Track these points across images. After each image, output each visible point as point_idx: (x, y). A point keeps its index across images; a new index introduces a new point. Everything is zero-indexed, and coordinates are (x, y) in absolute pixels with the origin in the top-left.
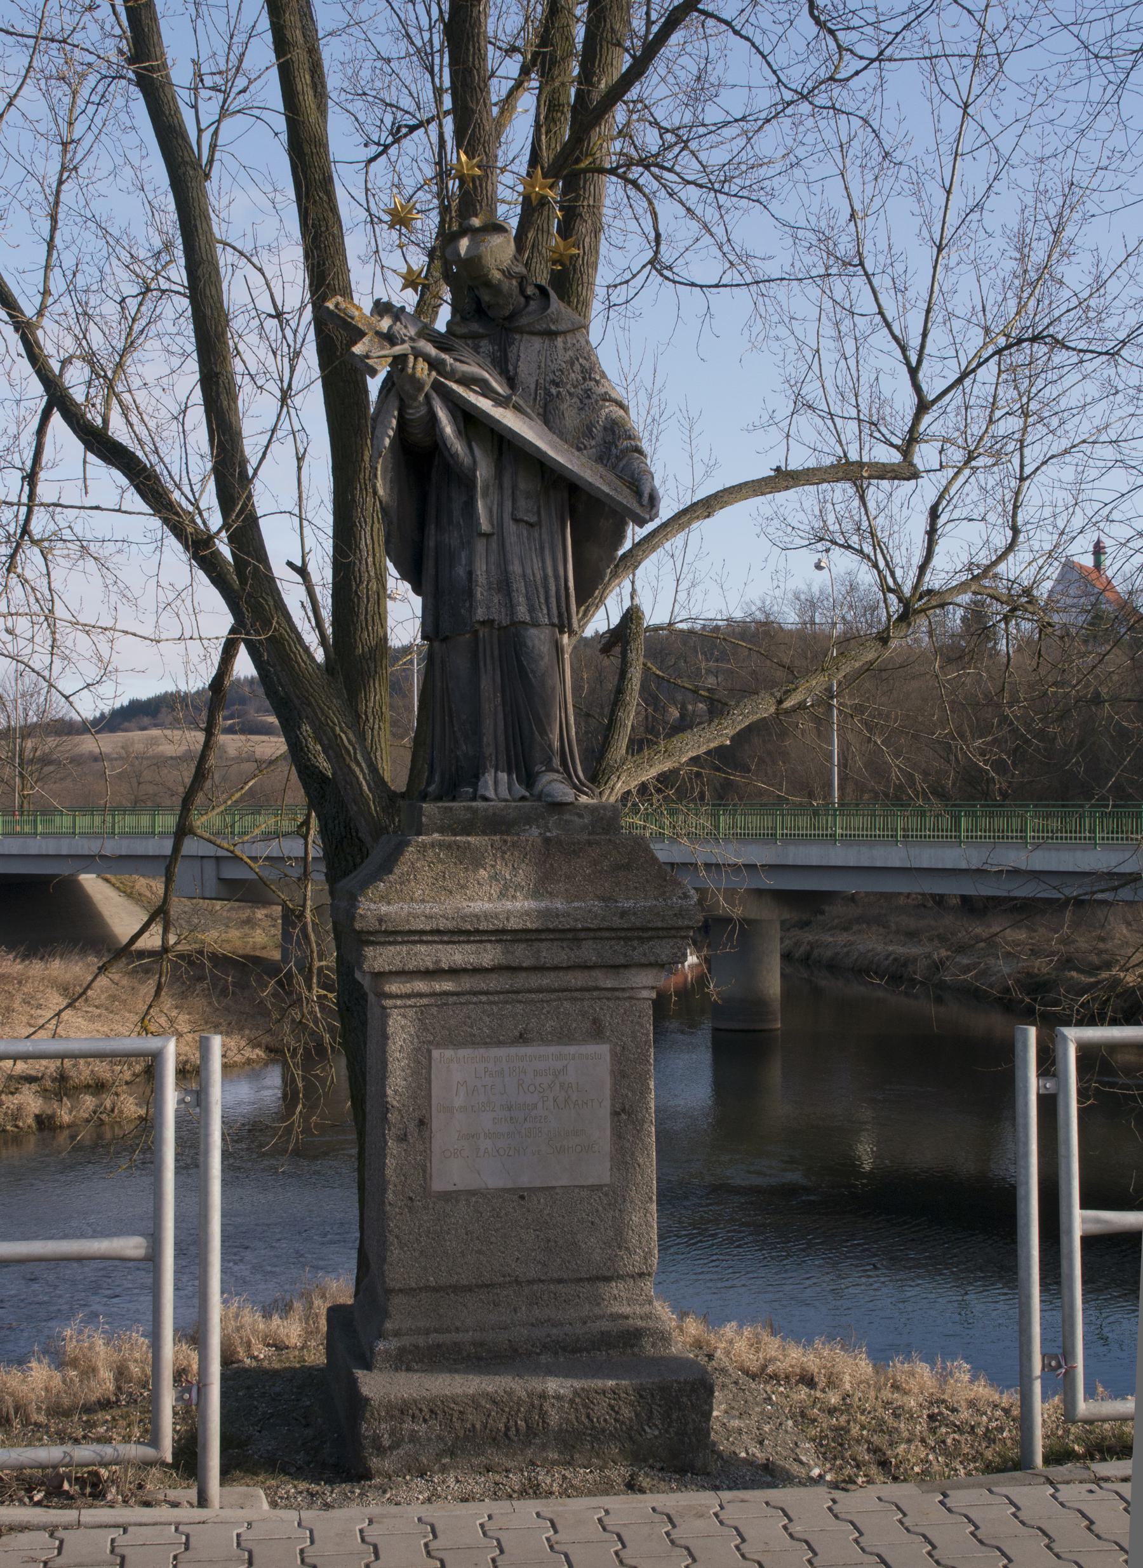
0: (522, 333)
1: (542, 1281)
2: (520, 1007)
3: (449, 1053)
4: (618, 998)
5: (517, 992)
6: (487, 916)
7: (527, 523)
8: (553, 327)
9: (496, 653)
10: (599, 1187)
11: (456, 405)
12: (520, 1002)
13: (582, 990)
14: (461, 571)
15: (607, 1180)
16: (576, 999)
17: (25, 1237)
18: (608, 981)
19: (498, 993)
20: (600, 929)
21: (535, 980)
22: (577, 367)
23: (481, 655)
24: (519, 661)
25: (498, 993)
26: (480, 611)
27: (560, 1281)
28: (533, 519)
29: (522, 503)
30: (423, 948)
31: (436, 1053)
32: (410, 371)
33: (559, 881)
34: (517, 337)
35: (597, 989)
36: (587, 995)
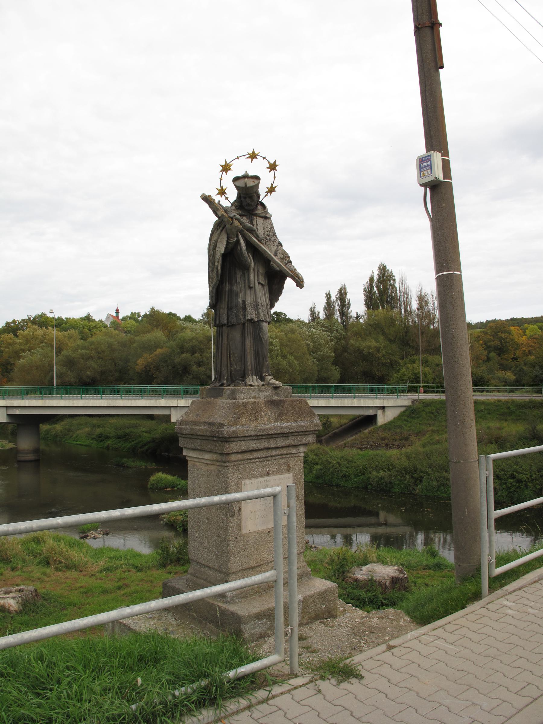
2: (267, 462)
16: (283, 458)
17: (58, 621)
18: (293, 451)
29: (260, 277)
30: (243, 443)
31: (243, 482)
32: (428, 190)
33: (283, 416)
34: (255, 217)
35: (291, 454)
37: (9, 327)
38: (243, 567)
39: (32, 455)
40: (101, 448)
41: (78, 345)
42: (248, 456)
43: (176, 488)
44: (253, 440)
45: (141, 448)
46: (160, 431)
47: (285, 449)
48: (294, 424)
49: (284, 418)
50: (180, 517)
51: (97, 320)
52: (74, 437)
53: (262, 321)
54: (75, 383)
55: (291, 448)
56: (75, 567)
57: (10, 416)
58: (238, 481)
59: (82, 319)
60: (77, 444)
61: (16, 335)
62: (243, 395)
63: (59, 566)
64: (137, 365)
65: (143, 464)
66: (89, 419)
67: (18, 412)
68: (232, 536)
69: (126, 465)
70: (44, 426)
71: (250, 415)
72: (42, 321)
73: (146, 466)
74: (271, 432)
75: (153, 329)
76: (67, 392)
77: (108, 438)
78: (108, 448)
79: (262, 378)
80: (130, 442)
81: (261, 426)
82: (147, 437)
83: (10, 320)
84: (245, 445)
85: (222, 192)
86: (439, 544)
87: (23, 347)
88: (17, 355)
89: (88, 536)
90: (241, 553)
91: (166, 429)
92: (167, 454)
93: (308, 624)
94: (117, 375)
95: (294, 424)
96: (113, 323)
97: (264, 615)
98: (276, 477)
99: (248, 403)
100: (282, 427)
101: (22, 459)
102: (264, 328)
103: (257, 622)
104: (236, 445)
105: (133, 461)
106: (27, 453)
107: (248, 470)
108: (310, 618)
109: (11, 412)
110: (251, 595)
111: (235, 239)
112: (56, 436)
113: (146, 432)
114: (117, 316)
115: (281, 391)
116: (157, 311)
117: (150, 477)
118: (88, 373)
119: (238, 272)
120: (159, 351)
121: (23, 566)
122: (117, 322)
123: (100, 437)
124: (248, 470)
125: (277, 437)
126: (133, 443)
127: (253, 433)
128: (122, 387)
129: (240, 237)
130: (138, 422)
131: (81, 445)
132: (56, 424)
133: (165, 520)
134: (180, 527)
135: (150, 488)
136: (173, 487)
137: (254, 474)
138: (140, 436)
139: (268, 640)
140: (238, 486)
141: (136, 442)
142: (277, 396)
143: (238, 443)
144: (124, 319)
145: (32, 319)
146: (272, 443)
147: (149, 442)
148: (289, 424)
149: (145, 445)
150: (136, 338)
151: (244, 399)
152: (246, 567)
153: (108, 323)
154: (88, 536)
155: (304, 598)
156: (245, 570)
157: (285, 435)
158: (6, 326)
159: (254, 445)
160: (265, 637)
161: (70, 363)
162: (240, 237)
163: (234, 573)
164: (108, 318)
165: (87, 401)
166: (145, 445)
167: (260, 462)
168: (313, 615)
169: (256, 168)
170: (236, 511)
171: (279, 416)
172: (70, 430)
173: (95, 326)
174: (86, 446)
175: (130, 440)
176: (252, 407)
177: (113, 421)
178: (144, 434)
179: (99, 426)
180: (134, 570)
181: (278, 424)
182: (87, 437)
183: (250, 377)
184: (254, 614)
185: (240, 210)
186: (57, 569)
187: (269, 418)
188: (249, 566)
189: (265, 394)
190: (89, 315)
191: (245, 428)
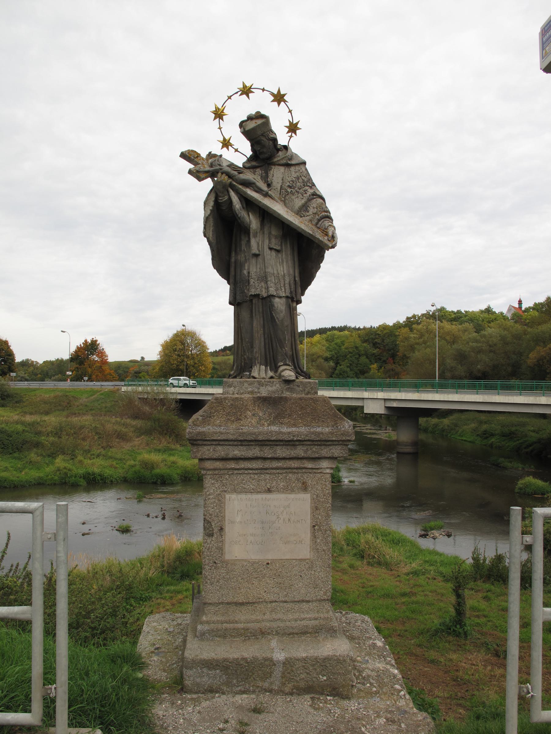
0: (275, 165)
1: (277, 602)
3: (234, 496)
4: (315, 473)
5: (266, 469)
6: (251, 434)
7: (276, 250)
8: (289, 162)
9: (261, 310)
10: (305, 560)
11: (241, 195)
12: (268, 474)
13: (297, 468)
14: (245, 272)
15: (308, 557)
16: (295, 473)
19: (257, 469)
20: (305, 441)
21: (275, 464)
22: (300, 180)
23: (254, 311)
24: (271, 314)
25: (257, 469)
26: (253, 290)
27: (285, 602)
28: (278, 248)
29: (273, 240)
30: (220, 448)
31: (227, 496)
33: (284, 418)
36: (300, 471)
37: (409, 321)
38: (225, 599)
39: (410, 447)
40: (485, 445)
41: (469, 338)
42: (233, 465)
44: (236, 445)
45: (525, 448)
47: (295, 461)
48: (303, 430)
49: (286, 420)
51: (497, 312)
52: (459, 432)
53: (273, 296)
54: (466, 377)
55: (305, 461)
56: (387, 565)
57: (388, 408)
58: (219, 495)
59: (482, 312)
60: (462, 440)
61: (411, 330)
62: (232, 388)
63: (371, 560)
65: (521, 466)
66: (477, 415)
67: (395, 405)
68: (209, 560)
69: (502, 465)
70: (433, 420)
71: (228, 414)
72: (441, 315)
74: (260, 438)
76: (390, 385)
77: (492, 435)
78: (491, 445)
79: (275, 368)
80: (515, 441)
81: (245, 429)
82: (534, 437)
83: (410, 316)
84: (221, 451)
85: (226, 144)
87: (417, 341)
88: (412, 348)
89: (427, 535)
93: (292, 694)
94: (510, 369)
95: (303, 430)
96: (514, 315)
97: (217, 665)
98: (282, 496)
99: (225, 398)
100: (281, 433)
101: (401, 451)
102: (276, 305)
103: (205, 670)
104: (209, 450)
105: (511, 462)
106: (406, 446)
107: (236, 482)
108: (295, 687)
109: (389, 404)
110: (231, 636)
111: (226, 198)
112: (443, 430)
113: (534, 431)
114: (520, 308)
115: (298, 386)
118: (479, 367)
119: (243, 237)
121: (340, 555)
122: (519, 315)
123: (485, 434)
124: (236, 482)
125: (277, 445)
126: (518, 442)
127: (231, 437)
128: (513, 382)
129: (232, 194)
130: (528, 420)
131: (465, 441)
132: (445, 418)
135: (518, 493)
137: (245, 488)
138: (526, 436)
139: (219, 697)
140: (219, 500)
141: (520, 441)
142: (291, 392)
143: (212, 448)
144: (527, 310)
145: (431, 313)
146: (267, 452)
147: (535, 443)
148: (294, 429)
149: (530, 446)
151: (233, 394)
152: (229, 600)
153: (509, 316)
154: (427, 535)
155: (286, 659)
156: (228, 603)
157: (291, 443)
158: (407, 321)
159: (237, 452)
160: (217, 692)
161: (461, 357)
162: (232, 194)
163: (210, 604)
164: (509, 310)
165: (462, 396)
167: (256, 474)
168: (302, 684)
169: (261, 103)
171: (278, 418)
172: (456, 425)
173: (495, 319)
174: (470, 442)
175: (515, 439)
176: (232, 405)
177: (501, 418)
179: (486, 423)
180: (441, 579)
181: (274, 428)
182: (472, 432)
183: (258, 366)
184: (201, 660)
185: (255, 161)
186: (369, 564)
187: (260, 419)
188: (235, 600)
189: (270, 389)
190: (489, 307)
191: (218, 430)
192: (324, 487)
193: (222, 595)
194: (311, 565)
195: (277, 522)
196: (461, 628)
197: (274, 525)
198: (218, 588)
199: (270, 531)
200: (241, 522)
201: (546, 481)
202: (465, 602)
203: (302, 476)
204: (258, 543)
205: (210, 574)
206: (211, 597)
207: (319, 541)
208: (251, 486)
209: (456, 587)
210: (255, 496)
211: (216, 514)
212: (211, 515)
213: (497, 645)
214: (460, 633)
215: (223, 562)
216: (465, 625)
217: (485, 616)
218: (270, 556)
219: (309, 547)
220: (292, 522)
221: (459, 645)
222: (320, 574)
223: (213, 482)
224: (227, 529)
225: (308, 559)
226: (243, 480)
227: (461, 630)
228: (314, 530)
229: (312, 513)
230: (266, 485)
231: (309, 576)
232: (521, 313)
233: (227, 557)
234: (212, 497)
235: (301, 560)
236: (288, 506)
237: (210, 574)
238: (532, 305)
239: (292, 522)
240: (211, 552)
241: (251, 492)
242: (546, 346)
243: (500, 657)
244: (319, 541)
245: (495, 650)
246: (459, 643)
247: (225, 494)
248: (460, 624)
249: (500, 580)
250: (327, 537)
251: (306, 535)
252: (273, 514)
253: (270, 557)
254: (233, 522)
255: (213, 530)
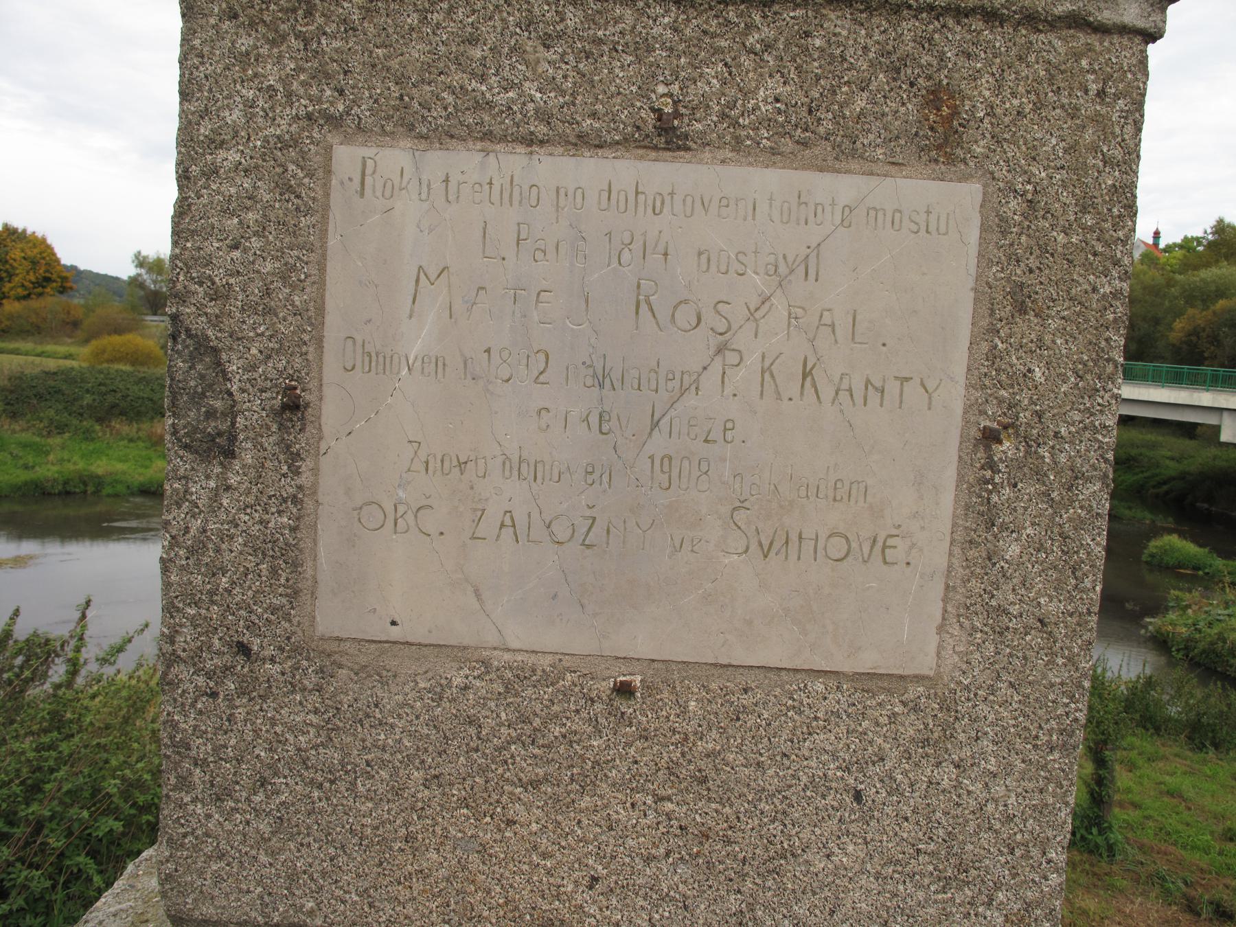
3: (394, 158)
15: (925, 664)
43: (1201, 573)
45: (1154, 487)
46: (1200, 460)
50: (1184, 630)
58: (284, 144)
64: (1171, 329)
73: (1154, 522)
75: (1217, 261)
82: (1172, 468)
86: (636, 207)
90: (288, 788)
91: (1215, 458)
92: (1206, 506)
98: (767, 182)
105: (1130, 508)
113: (1172, 459)
114: (1156, 245)
116: (1229, 226)
117: (1149, 541)
120: (1221, 304)
124: (417, 51)
126: (1141, 475)
130: (1160, 438)
133: (1150, 628)
134: (1178, 650)
135: (1147, 562)
136: (1196, 568)
140: (285, 188)
141: (1146, 475)
144: (1169, 249)
147: (1174, 479)
149: (1165, 483)
150: (1178, 277)
166: (1165, 483)
170: (254, 411)
175: (1137, 470)
178: (1167, 462)
192: (1089, 135)
193: (293, 877)
194: (937, 715)
195: (710, 381)
196: (1100, 833)
197: (690, 400)
198: (265, 827)
199: (659, 444)
200: (439, 364)
201: (1201, 546)
202: (1113, 777)
203: (925, 42)
204: (562, 532)
205: (208, 725)
206: (218, 879)
207: (1014, 550)
208: (531, 88)
209: (1096, 743)
210: (555, 170)
211: (255, 289)
212: (219, 295)
213: (1186, 883)
214: (1097, 846)
215: (297, 650)
216: (1110, 827)
217: (1136, 806)
218: (643, 638)
219: (937, 589)
220: (827, 392)
221: (1095, 874)
222: (998, 790)
223: (244, 43)
224: (331, 411)
225: (919, 679)
226: (473, 41)
227: (1099, 840)
228: (991, 465)
229: (988, 329)
230: (644, 93)
231: (916, 799)
232: (1156, 253)
233: (331, 617)
234: (233, 156)
235: (868, 682)
236: (808, 265)
237: (208, 725)
238: (1178, 241)
239: (827, 392)
240: (215, 571)
241: (530, 141)
242: (1208, 308)
243: (1199, 915)
244: (1014, 550)
245: (1184, 895)
246: (1096, 869)
247: (333, 138)
248: (1098, 825)
249: (1149, 725)
250: (1079, 524)
251: (925, 501)
252: (685, 316)
253: (644, 648)
254: (378, 361)
255: (232, 412)
